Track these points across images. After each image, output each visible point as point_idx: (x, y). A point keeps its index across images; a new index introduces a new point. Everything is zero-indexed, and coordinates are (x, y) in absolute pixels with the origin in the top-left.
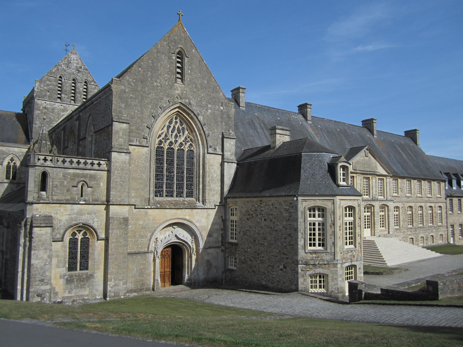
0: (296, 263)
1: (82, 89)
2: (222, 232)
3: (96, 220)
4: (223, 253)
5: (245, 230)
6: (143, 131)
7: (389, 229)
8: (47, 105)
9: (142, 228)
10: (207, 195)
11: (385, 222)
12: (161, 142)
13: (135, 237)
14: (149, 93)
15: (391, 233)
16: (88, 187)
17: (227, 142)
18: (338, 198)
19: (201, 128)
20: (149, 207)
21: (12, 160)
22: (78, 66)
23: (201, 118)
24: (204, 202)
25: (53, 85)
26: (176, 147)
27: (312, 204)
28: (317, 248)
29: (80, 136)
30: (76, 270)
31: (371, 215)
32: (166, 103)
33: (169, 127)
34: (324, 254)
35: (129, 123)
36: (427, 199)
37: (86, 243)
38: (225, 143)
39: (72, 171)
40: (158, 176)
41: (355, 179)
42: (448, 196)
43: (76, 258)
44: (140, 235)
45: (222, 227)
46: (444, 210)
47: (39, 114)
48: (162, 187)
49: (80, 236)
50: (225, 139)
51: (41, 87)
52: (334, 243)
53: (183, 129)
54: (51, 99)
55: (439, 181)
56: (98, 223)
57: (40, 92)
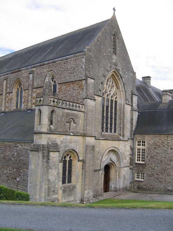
2: (131, 156)
3: (78, 147)
4: (131, 170)
5: (153, 155)
10: (125, 132)
16: (74, 123)
20: (102, 139)
24: (123, 136)
29: (34, 85)
30: (65, 183)
35: (94, 79)
39: (66, 111)
44: (97, 158)
49: (68, 159)
50: (134, 96)
56: (80, 149)
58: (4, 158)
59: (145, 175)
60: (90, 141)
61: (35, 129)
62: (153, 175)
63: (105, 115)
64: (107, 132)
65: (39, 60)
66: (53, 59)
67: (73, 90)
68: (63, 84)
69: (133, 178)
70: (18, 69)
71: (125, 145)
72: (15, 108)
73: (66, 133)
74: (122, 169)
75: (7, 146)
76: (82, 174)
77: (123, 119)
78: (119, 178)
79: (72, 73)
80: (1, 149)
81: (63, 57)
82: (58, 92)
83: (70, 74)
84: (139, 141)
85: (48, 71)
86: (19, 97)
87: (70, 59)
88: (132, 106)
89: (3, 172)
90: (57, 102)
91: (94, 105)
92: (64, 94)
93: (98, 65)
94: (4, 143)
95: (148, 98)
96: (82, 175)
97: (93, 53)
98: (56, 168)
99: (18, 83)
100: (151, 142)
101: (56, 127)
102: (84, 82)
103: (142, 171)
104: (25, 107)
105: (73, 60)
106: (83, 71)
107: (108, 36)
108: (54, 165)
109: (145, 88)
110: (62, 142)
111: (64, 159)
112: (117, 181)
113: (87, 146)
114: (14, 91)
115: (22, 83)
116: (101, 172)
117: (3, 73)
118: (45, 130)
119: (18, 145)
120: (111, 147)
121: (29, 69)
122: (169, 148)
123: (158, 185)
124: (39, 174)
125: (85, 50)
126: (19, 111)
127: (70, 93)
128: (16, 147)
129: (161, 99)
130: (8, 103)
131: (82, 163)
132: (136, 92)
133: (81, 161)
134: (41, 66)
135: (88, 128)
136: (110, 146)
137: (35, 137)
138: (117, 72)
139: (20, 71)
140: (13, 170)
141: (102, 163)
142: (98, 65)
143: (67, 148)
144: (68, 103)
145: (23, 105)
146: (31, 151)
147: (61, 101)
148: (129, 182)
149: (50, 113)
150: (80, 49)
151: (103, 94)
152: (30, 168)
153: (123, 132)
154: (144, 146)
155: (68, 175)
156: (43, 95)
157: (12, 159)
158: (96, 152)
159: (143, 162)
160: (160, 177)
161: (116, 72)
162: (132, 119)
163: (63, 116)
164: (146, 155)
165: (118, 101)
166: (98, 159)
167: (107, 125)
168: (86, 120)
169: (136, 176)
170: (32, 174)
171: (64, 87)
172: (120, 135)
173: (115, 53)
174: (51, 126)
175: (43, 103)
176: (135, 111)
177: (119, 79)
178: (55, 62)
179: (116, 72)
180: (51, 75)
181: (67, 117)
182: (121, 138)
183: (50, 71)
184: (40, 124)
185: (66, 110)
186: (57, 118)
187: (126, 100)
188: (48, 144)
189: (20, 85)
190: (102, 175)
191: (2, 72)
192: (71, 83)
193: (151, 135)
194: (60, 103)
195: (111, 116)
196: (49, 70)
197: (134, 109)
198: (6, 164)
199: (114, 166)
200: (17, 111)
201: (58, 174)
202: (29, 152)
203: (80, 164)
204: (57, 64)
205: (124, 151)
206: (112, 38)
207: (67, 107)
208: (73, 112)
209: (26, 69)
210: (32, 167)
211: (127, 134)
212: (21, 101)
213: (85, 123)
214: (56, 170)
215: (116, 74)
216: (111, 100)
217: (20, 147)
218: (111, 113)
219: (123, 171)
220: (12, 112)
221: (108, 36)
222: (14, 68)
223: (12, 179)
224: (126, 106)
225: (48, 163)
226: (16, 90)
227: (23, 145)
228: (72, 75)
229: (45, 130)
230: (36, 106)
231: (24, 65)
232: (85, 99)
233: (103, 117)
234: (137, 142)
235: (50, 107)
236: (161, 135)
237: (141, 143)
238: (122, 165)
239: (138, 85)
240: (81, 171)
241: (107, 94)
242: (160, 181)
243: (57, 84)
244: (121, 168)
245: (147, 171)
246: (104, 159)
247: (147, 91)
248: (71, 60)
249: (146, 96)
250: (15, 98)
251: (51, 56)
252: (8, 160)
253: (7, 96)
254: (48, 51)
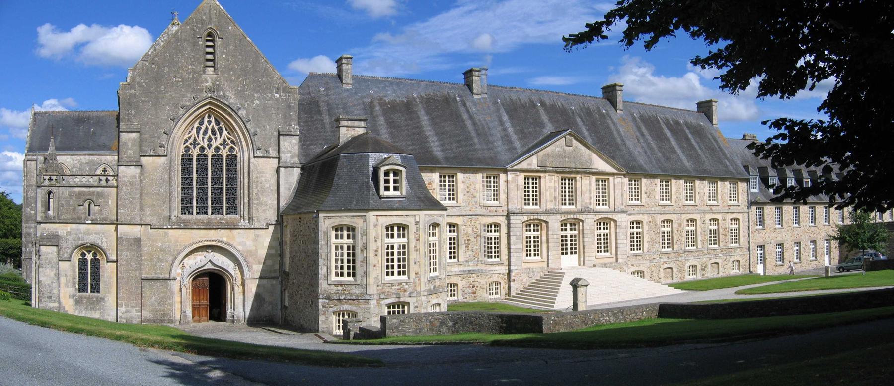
0: (317, 297)
3: (104, 240)
6: (159, 138)
7: (617, 255)
9: (161, 250)
11: (604, 244)
12: (187, 149)
13: (151, 260)
14: (167, 92)
15: (620, 261)
17: (284, 140)
18: (371, 213)
19: (243, 126)
23: (242, 113)
26: (210, 153)
27: (337, 221)
28: (345, 278)
31: (579, 234)
32: (189, 101)
33: (199, 129)
34: (353, 287)
36: (708, 208)
37: (96, 264)
38: (281, 142)
40: (186, 189)
41: (542, 180)
42: (752, 203)
43: (87, 279)
46: (743, 226)
48: (192, 203)
49: (89, 257)
50: (281, 137)
52: (365, 273)
53: (220, 129)
55: (734, 179)
98: (52, 267)
165: (238, 155)
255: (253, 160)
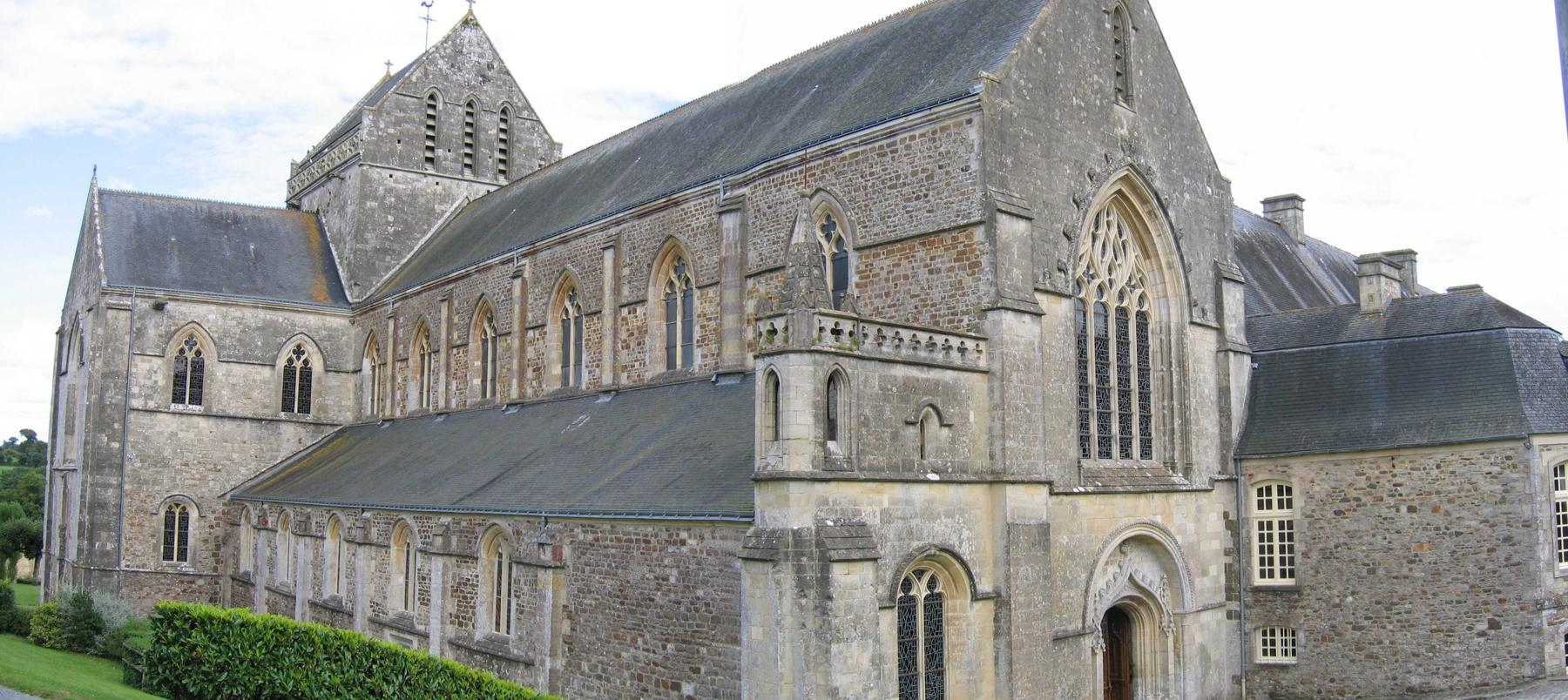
1: (494, 131)
2: (1229, 560)
3: (966, 534)
4: (1235, 622)
8: (396, 181)
16: (942, 425)
21: (299, 351)
22: (483, 61)
24: (1187, 471)
25: (413, 121)
39: (900, 371)
44: (1064, 579)
45: (1230, 545)
47: (373, 210)
49: (920, 591)
50: (1225, 285)
51: (378, 129)
54: (405, 162)
56: (976, 542)
57: (376, 143)
58: (621, 594)
59: (1301, 636)
60: (1028, 502)
61: (758, 463)
62: (1339, 634)
63: (1092, 379)
64: (1108, 455)
65: (759, 150)
66: (827, 139)
67: (931, 272)
68: (879, 250)
69: (1247, 654)
70: (664, 195)
71: (1199, 510)
72: (661, 368)
73: (905, 476)
74: (1189, 621)
75: (630, 541)
76: (996, 658)
77: (1183, 393)
78: (1177, 662)
79: (918, 198)
80: (607, 556)
81: (870, 126)
82: (857, 286)
83: (909, 200)
84: (1264, 485)
85: (803, 196)
86: (679, 318)
87: (907, 135)
88: (1220, 331)
89: (618, 656)
90: (851, 334)
91: (1036, 338)
92: (887, 294)
93: (1047, 154)
94: (619, 528)
95: (1293, 292)
96: (996, 664)
97: (1018, 101)
98: (864, 636)
99: (669, 257)
100: (1320, 489)
101: (854, 447)
102: (979, 234)
103: (1288, 621)
104: (710, 361)
105: (922, 135)
106: (973, 184)
107: (1086, 17)
108: (857, 621)
109: (1280, 247)
110: (887, 516)
111: (900, 594)
112: (1172, 677)
113: (1010, 528)
114: (655, 295)
115: (688, 258)
116: (1088, 642)
117: (598, 219)
118: (800, 462)
119: (684, 535)
120: (1127, 528)
121: (717, 191)
122: (1404, 509)
123: (1361, 673)
124: (785, 667)
125: (979, 87)
126: (684, 383)
127: (916, 290)
128: (675, 543)
129: (1357, 297)
130: (628, 347)
131: (990, 605)
132: (1234, 267)
133: (986, 597)
134: (768, 173)
135: (1009, 444)
136: (1125, 521)
137: (763, 499)
138: (1139, 181)
139: (677, 204)
140: (664, 647)
141: (1090, 600)
142: (1047, 154)
143: (915, 544)
144: (906, 335)
145: (698, 353)
146: (745, 559)
147: (872, 330)
148: (1227, 675)
149: (822, 387)
150: (952, 85)
151: (1079, 284)
152: (744, 639)
153: (1186, 452)
154: (1290, 505)
155: (928, 665)
156: (785, 303)
157: (659, 597)
158: (1056, 552)
159: (1288, 582)
160: (1371, 636)
161: (1137, 180)
162: (1224, 392)
163: (885, 395)
164: (1299, 547)
165: (1152, 314)
166: (1068, 584)
167: (1104, 426)
168: (999, 406)
169: (1260, 648)
170: (754, 664)
171: (883, 263)
172: (1173, 468)
173: (1125, 93)
174: (831, 445)
175: (786, 341)
176: (1235, 352)
177: (1149, 213)
178: (833, 152)
179: (1137, 180)
180: (818, 212)
181: (908, 401)
182: (1178, 478)
183: (811, 197)
184: (776, 438)
185: (899, 367)
186: (859, 406)
187: (1192, 304)
188: (820, 527)
189: (679, 264)
190: (1094, 653)
191: (593, 216)
192: (916, 243)
193: (1316, 459)
194: (865, 335)
195: (1124, 381)
196: (808, 191)
197: (1230, 346)
198: (630, 622)
199: (1147, 605)
200: (675, 382)
201: (877, 661)
202: (739, 564)
203: (985, 610)
204: (844, 158)
205: (1194, 539)
206: (1108, 26)
207: (905, 353)
208: (934, 374)
209: (703, 195)
210: (753, 632)
211: (1207, 457)
212: (688, 336)
213: (998, 424)
214: (864, 648)
215: (1134, 188)
216: (1117, 309)
217: (692, 542)
218: (1123, 369)
219: (1194, 628)
220: (651, 386)
221: (1086, 17)
222: (646, 194)
223: (662, 689)
224: (1193, 334)
225: (825, 612)
226: (663, 288)
227: (707, 535)
228: (920, 203)
229: (800, 462)
230: (756, 357)
231: (691, 179)
232: (989, 314)
233: (1083, 388)
234: (1254, 493)
235: (818, 357)
236: (1362, 451)
237: (1275, 497)
238: (1190, 603)
239: (1244, 235)
240: (988, 645)
241: (1097, 282)
242: (1369, 656)
243: (849, 248)
244: (1183, 615)
245: (1307, 619)
246: (1099, 583)
247: (1289, 263)
248: (913, 138)
249: (1287, 284)
250: (658, 327)
251: (816, 128)
252: (638, 605)
253: (624, 319)
254: (798, 107)
255: (1189, 330)
